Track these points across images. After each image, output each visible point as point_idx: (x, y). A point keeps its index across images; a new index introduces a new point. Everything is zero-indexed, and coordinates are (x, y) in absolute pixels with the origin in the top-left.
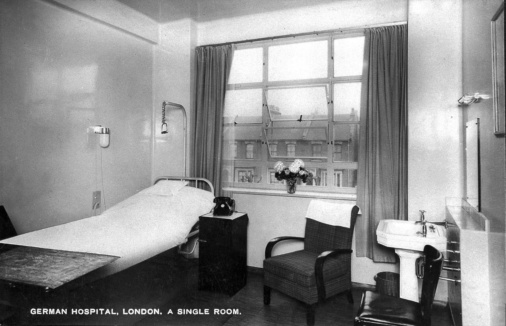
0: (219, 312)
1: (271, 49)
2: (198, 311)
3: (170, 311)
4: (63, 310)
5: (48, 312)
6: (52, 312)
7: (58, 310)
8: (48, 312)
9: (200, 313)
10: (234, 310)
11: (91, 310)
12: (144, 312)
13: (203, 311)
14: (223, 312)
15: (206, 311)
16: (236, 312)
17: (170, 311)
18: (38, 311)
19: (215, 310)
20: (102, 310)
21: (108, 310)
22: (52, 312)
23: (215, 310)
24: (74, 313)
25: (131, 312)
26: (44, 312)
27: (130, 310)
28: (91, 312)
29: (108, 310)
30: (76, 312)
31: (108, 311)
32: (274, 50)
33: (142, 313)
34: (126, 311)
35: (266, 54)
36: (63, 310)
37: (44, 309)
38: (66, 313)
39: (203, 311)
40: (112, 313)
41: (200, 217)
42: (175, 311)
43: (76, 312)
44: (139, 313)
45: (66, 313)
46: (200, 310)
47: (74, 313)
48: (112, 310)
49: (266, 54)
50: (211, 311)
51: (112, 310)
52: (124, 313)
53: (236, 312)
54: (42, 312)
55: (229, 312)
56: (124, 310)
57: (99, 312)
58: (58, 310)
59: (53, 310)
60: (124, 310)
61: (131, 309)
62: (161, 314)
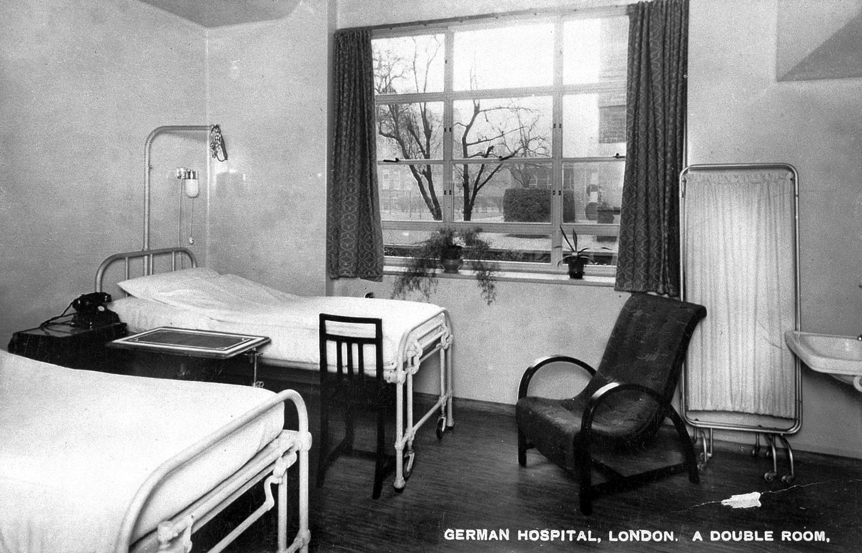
0: (791, 537)
1: (457, 35)
2: (754, 535)
3: (697, 536)
4: (501, 532)
5: (476, 536)
6: (482, 534)
7: (493, 532)
8: (476, 536)
9: (757, 539)
10: (638, 539)
11: (553, 532)
12: (646, 536)
13: (761, 535)
14: (797, 536)
15: (768, 536)
16: (820, 536)
17: (697, 536)
18: (457, 534)
19: (783, 533)
20: (571, 532)
21: (582, 533)
22: (482, 534)
23: (783, 533)
24: (523, 538)
25: (623, 536)
26: (468, 535)
27: (621, 534)
28: (553, 536)
29: (582, 533)
30: (525, 535)
31: (582, 536)
32: (463, 37)
33: (643, 539)
34: (615, 535)
35: (559, 68)
36: (501, 532)
37: (468, 531)
38: (507, 538)
39: (761, 535)
40: (590, 539)
41: (700, 313)
42: (706, 536)
43: (525, 535)
44: (638, 539)
45: (507, 538)
46: (756, 533)
47: (523, 538)
48: (590, 532)
49: (559, 68)
50: (777, 536)
51: (590, 532)
52: (611, 539)
53: (820, 536)
54: (465, 534)
55: (808, 536)
56: (611, 533)
57: (567, 536)
58: (493, 532)
59: (485, 531)
60: (611, 533)
61: (658, 532)
62: (828, 540)
